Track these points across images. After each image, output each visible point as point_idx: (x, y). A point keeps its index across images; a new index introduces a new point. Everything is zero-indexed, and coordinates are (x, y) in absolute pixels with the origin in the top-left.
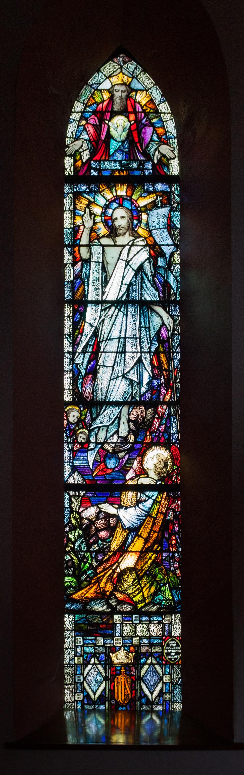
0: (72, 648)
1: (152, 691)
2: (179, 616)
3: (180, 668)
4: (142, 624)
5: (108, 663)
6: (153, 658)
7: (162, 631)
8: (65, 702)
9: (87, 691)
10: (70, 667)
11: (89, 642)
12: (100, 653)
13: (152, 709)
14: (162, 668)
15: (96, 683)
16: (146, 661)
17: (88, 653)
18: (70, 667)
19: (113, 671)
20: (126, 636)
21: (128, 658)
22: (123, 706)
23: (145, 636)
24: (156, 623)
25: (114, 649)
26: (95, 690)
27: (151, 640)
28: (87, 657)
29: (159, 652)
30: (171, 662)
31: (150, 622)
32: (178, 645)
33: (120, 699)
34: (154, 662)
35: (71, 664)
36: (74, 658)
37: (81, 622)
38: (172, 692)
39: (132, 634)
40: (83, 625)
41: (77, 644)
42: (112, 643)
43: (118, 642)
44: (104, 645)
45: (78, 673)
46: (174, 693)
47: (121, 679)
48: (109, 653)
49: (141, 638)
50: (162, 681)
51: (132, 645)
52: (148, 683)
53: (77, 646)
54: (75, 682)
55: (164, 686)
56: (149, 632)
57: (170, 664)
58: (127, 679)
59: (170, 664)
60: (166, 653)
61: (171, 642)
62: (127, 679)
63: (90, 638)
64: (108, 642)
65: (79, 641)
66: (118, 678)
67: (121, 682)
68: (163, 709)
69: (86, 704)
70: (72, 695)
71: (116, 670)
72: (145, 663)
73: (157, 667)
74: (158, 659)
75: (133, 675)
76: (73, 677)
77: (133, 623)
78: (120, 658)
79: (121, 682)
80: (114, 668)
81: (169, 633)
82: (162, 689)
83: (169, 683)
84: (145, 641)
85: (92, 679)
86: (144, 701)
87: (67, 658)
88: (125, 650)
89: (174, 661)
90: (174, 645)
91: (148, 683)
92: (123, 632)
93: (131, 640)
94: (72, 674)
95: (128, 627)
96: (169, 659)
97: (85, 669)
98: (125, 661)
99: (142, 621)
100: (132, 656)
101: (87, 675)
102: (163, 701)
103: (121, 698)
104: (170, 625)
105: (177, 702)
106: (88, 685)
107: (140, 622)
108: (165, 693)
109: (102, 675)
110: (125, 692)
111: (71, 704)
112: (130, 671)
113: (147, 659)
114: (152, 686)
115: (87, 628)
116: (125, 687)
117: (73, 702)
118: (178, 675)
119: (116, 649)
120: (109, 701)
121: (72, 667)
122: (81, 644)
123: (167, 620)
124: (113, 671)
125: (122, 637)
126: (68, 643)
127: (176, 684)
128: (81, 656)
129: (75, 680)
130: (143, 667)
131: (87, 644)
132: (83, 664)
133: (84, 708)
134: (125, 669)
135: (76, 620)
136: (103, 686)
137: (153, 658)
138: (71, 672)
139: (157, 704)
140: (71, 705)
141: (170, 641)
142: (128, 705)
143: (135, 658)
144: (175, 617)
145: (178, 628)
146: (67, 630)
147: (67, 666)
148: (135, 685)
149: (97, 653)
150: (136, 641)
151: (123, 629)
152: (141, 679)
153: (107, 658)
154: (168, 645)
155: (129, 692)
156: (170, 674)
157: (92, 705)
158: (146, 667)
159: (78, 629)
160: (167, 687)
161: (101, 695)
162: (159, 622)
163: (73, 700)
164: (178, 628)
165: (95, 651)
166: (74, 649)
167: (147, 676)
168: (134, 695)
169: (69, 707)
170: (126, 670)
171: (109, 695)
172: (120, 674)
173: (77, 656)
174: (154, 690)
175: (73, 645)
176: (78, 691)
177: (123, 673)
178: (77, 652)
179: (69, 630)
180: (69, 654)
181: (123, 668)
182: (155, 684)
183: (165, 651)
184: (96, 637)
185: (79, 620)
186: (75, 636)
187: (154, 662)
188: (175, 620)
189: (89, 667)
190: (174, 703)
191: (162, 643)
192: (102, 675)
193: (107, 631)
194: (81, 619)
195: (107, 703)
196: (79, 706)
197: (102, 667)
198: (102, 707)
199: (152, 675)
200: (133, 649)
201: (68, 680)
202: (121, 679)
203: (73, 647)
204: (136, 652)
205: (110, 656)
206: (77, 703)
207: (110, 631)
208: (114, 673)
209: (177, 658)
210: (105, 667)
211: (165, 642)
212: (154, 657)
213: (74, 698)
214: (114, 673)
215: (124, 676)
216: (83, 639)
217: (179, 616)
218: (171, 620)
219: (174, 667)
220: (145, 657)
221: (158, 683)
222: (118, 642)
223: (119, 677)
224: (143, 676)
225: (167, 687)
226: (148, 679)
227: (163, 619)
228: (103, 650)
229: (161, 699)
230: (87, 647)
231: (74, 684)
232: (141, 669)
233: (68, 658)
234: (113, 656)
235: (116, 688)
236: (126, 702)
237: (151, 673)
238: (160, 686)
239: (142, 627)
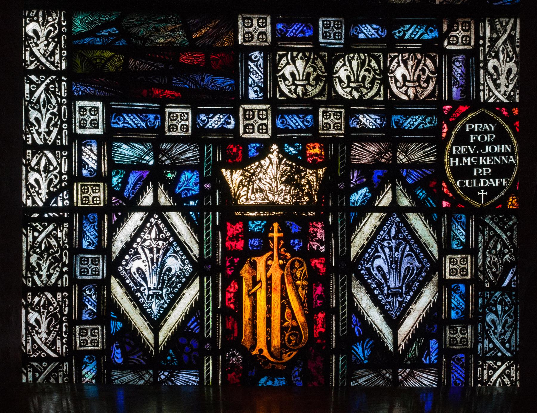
0: (62, 148)
1: (394, 314)
2: (512, 27)
3: (511, 229)
4: (358, 51)
5: (214, 208)
7: (439, 81)
8: (26, 359)
9: (122, 316)
10: (50, 220)
11: (133, 121)
12: (179, 168)
13: (395, 382)
14: (435, 226)
15: (161, 283)
16: (373, 199)
17: (128, 169)
18: (50, 220)
19: (236, 238)
20: (289, 101)
21: (298, 186)
22: (273, 374)
23: (371, 102)
24: (414, 51)
25: (239, 152)
26: (155, 309)
27: (395, 118)
28: (125, 182)
29: (427, 166)
30: (473, 202)
31: (391, 46)
32: (501, 138)
33: (261, 343)
34: (405, 202)
35: (57, 210)
36: (70, 189)
37: (99, 42)
38: (474, 318)
39: (313, 91)
40: (108, 54)
41: (79, 131)
42: (232, 126)
43: (254, 123)
44: (198, 136)
45: (85, 244)
46: (484, 321)
47: (268, 267)
48: (217, 167)
49: (351, 108)
50: (435, 278)
51: (316, 138)
52: (379, 286)
53: (83, 140)
54: (73, 280)
55: (445, 295)
56: (387, 87)
57: (469, 211)
58: (292, 266)
59: (469, 211)
60: (453, 169)
61: (476, 127)
62: (292, 266)
63: (138, 105)
64: (215, 122)
65: (89, 118)
66: (254, 266)
67: (269, 280)
68: (439, 382)
69: (119, 367)
70: (59, 333)
71: (248, 235)
72: (369, 206)
73: (417, 222)
74: (421, 194)
75: (317, 254)
76: (66, 259)
77: (317, 49)
78: (264, 184)
79: (269, 280)
80: (239, 226)
81: (465, 91)
82: (435, 308)
83: (466, 283)
84: (369, 121)
85: (145, 269)
86: (360, 351)
87: (37, 183)
88: (287, 155)
89: (487, 199)
90: (487, 138)
91: (379, 286)
92: (276, 84)
93: (309, 118)
94: (61, 248)
95: (300, 64)
96: (465, 190)
97: (114, 229)
98: (283, 197)
99: (356, 39)
100: (312, 178)
101: (125, 251)
102: (441, 352)
103: (269, 343)
104: (472, 61)
105: (495, 358)
106: (130, 293)
107: (351, 45)
108: (450, 322)
109: (186, 253)
110: (283, 319)
111: (53, 366)
112: (306, 236)
113: (376, 192)
114: (395, 295)
115: (126, 64)
116: (284, 297)
117: (61, 359)
118: (501, 254)
119: (246, 151)
120: (214, 353)
121: (59, 222)
122: (99, 131)
123: (459, 39)
124: (236, 238)
125: (274, 102)
126: (40, 125)
127: (496, 286)
128: (97, 177)
129: (71, 273)
130: (358, 221)
131: (125, 131)
132: (108, 208)
133: (111, 382)
134: (283, 229)
135: (76, 30)
136: (191, 294)
138: (54, 242)
139: (418, 365)
140: (56, 370)
141: (472, 121)
142: (296, 372)
143: (325, 185)
144: (493, 30)
145: (503, 69)
146: (37, 72)
147: (41, 219)
148: (327, 291)
149: (167, 167)
150: (332, 120)
151: (276, 69)
153: (208, 186)
154: (462, 138)
155: (300, 319)
156: (469, 249)
157: (146, 368)
158: (372, 221)
159: (83, 73)
160: (457, 300)
161: (182, 328)
162: (428, 48)
164: (503, 69)
165: (156, 159)
166: (69, 149)
168: (320, 329)
169: (48, 378)
171: (215, 329)
172: (265, 248)
173: (81, 178)
174: (405, 312)
175: (65, 132)
176: (86, 317)
177: (275, 245)
178: (82, 165)
179: (48, 72)
180: (47, 170)
181: (276, 225)
182: (409, 287)
183: (449, 162)
184: (163, 103)
185: (91, 33)
186: (72, 98)
188: (494, 41)
189: (135, 219)
190: (485, 359)
191: (439, 128)
192: (186, 253)
193: (207, 79)
194: (99, 29)
195: (208, 365)
196: (89, 373)
197: (189, 220)
198: (187, 378)
199: (397, 255)
200: (317, 151)
201: (44, 273)
202: (268, 268)
203: (65, 142)
204: (329, 163)
205: (223, 177)
206: (80, 365)
207: (220, 80)
208: (240, 245)
209: (501, 187)
210: (200, 220)
211: (451, 128)
212: (406, 186)
213: (69, 343)
214: (240, 245)
215: (280, 257)
216: (109, 113)
217: (512, 27)
218: (477, 37)
219: (485, 225)
220: (369, 184)
221: (423, 285)
222: (254, 123)
223: (261, 262)
224: (360, 257)
225: (457, 300)
226: (379, 268)
227: (443, 36)
228: (190, 154)
229: (433, 344)
230: (127, 141)
231: (68, 289)
232: (353, 227)
233: (44, 185)
234: (234, 178)
235: (247, 303)
236: (286, 358)
237: (393, 244)
238: (428, 296)
239: (355, 63)
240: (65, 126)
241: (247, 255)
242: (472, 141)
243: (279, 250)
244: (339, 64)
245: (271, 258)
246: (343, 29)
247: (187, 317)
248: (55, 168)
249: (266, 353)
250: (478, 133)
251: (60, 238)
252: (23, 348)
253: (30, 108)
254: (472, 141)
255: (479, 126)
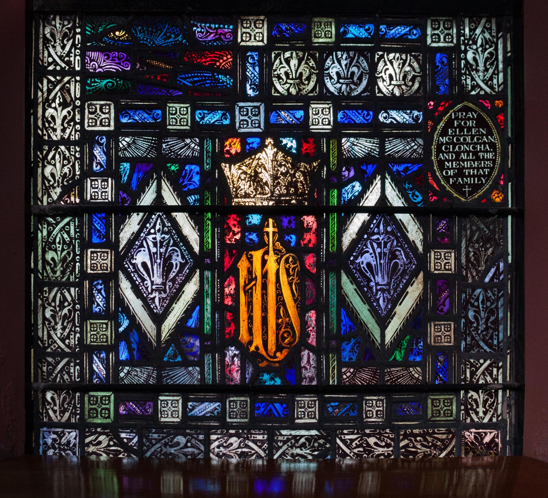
6: (388, 182)
34: (395, 199)
43: (249, 118)
66: (250, 260)
79: (265, 276)
90: (470, 123)
101: (131, 243)
106: (136, 289)
136: (191, 289)
137: (388, 182)
152: (340, 261)
161: (181, 327)
163: (73, 341)
167: (362, 253)
170: (281, 234)
172: (262, 244)
187: (395, 199)
215: (277, 251)
223: (257, 255)
238: (415, 291)
240: (78, 52)
241: (244, 248)
242: (455, 125)
243: (274, 244)
244: (329, 62)
245: (267, 253)
246: (444, 272)
247: (188, 313)
248: (69, 305)
249: (262, 351)
250: (462, 119)
251: (72, 373)
252: (39, 342)
253: (46, 164)
254: (455, 125)
255: (462, 114)
